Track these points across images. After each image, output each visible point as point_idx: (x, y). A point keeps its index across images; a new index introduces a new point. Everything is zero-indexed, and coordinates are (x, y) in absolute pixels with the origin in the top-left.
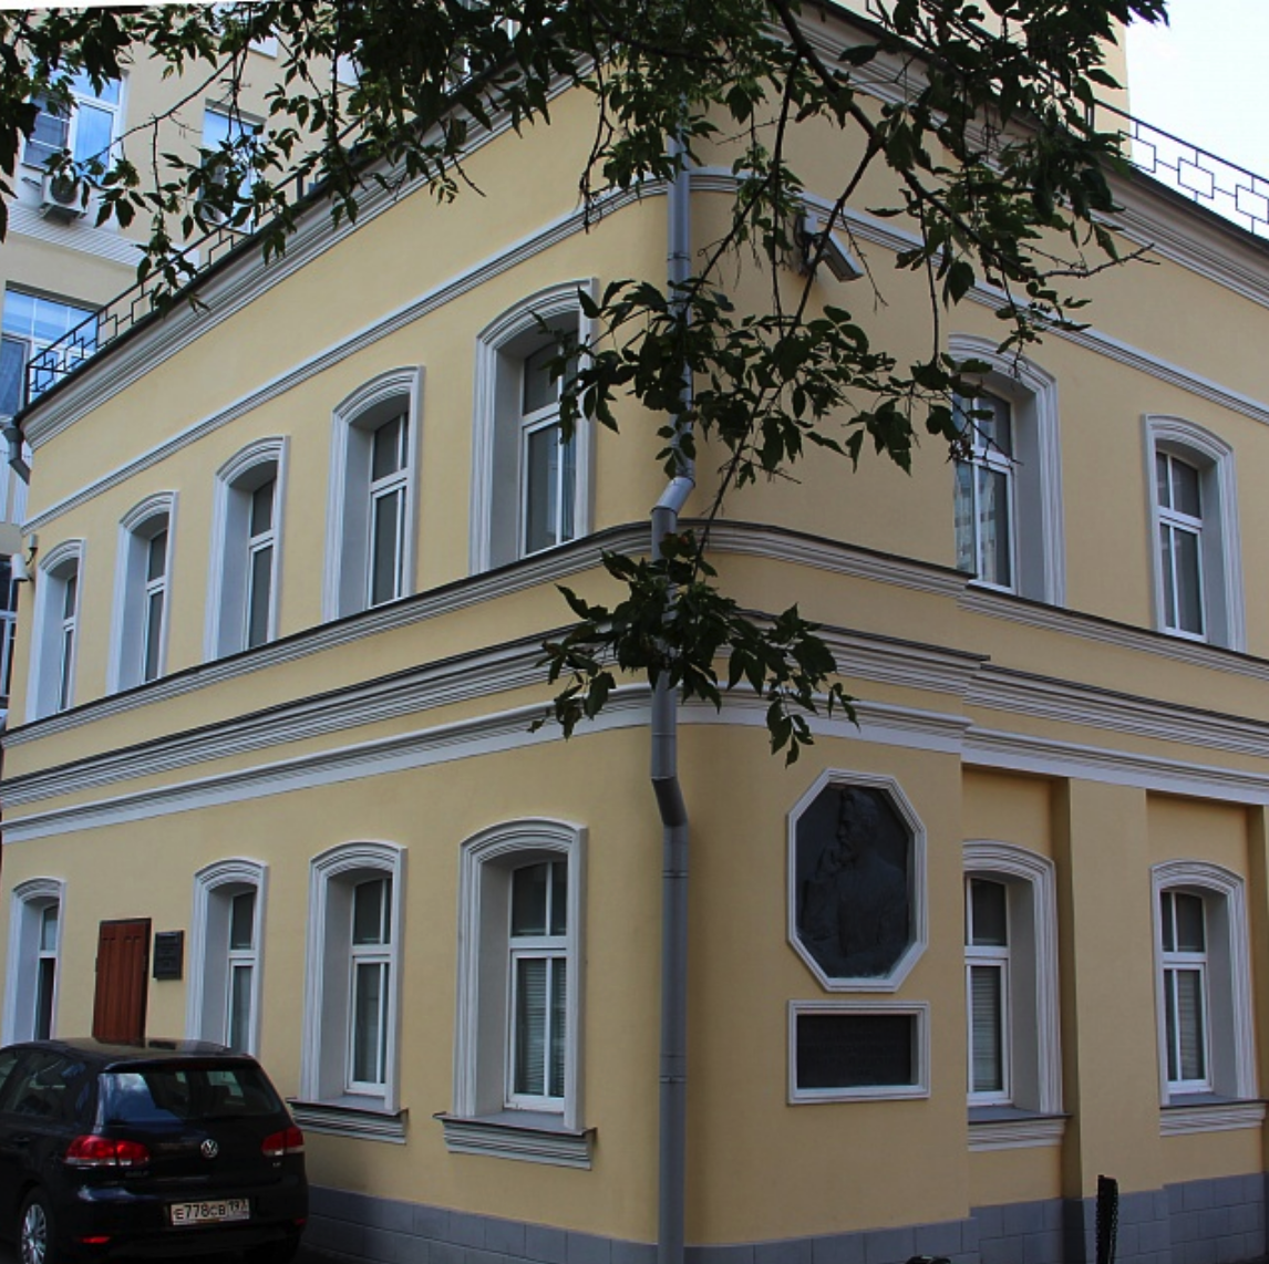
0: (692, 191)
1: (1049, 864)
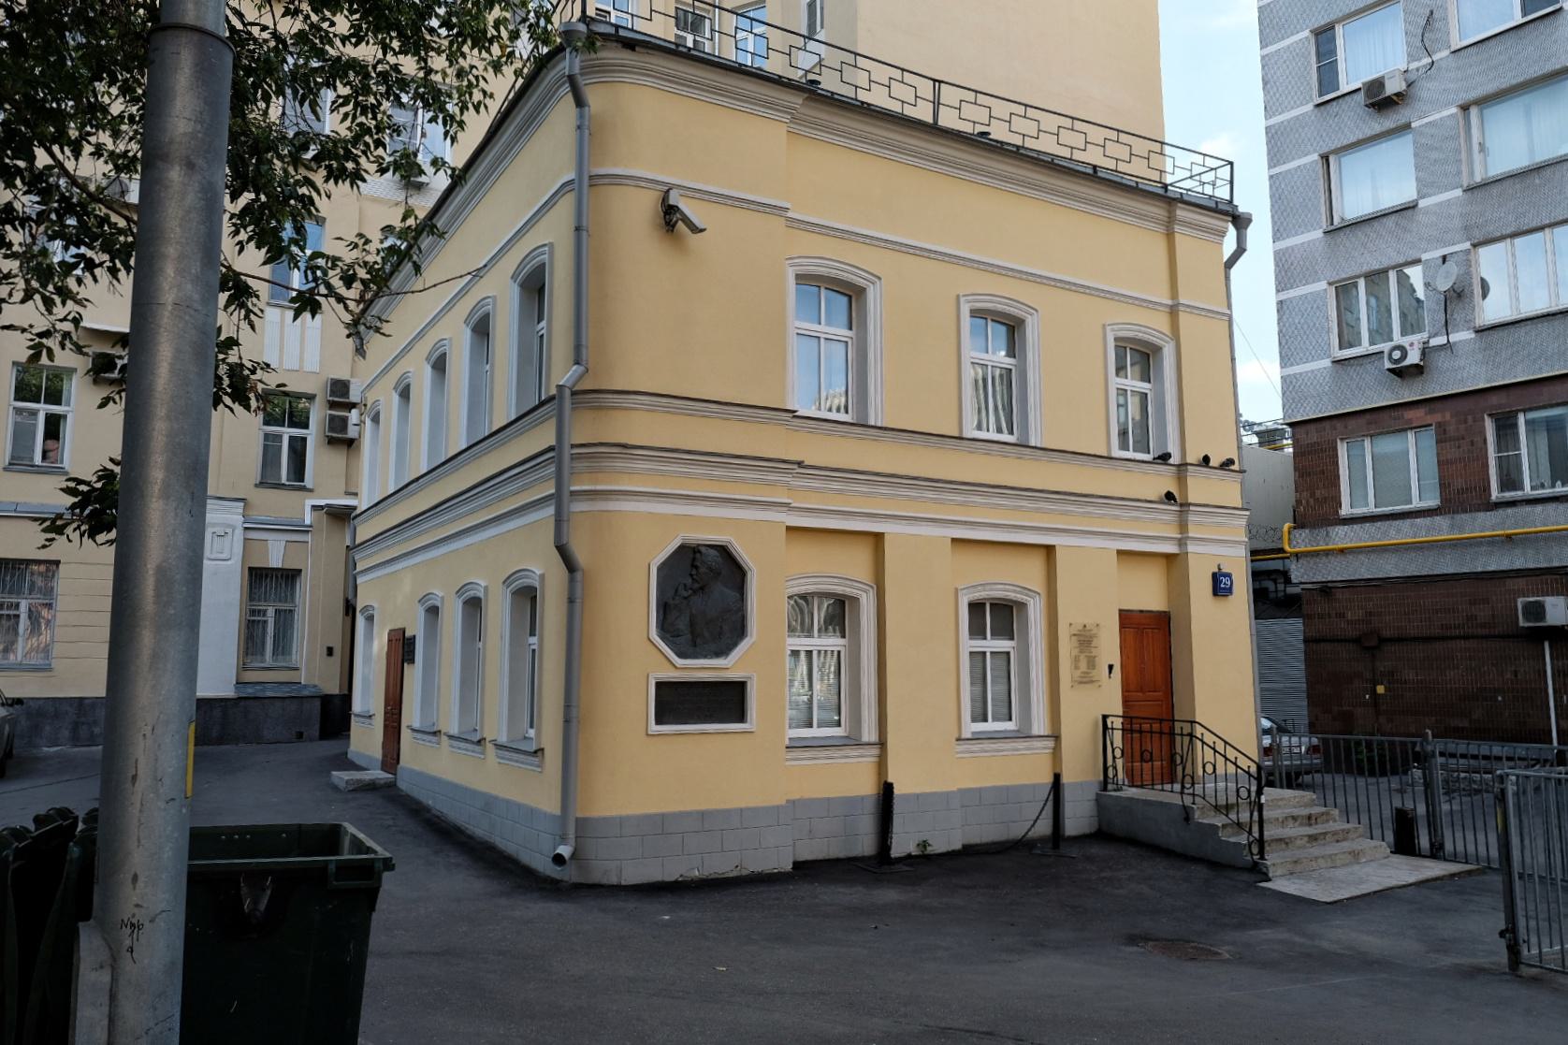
0: (591, 186)
1: (872, 587)
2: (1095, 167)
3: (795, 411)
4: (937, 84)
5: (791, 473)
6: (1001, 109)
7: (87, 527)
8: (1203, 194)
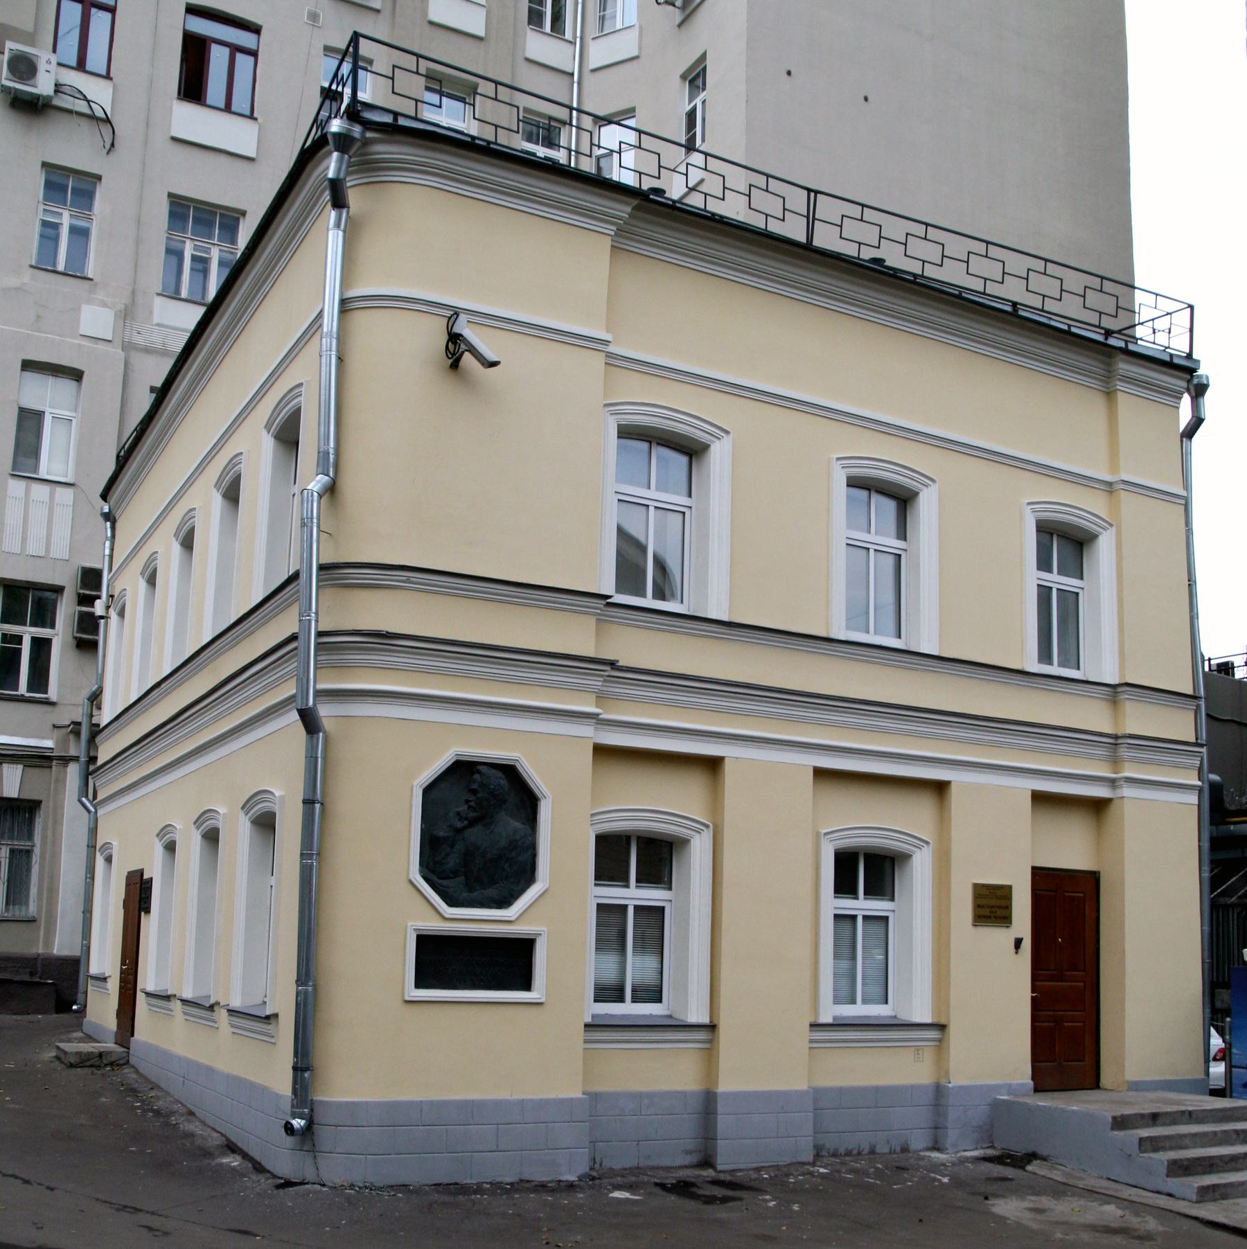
2: (1014, 304)
3: (610, 597)
4: (812, 195)
5: (602, 676)
6: (896, 229)
8: (1154, 343)
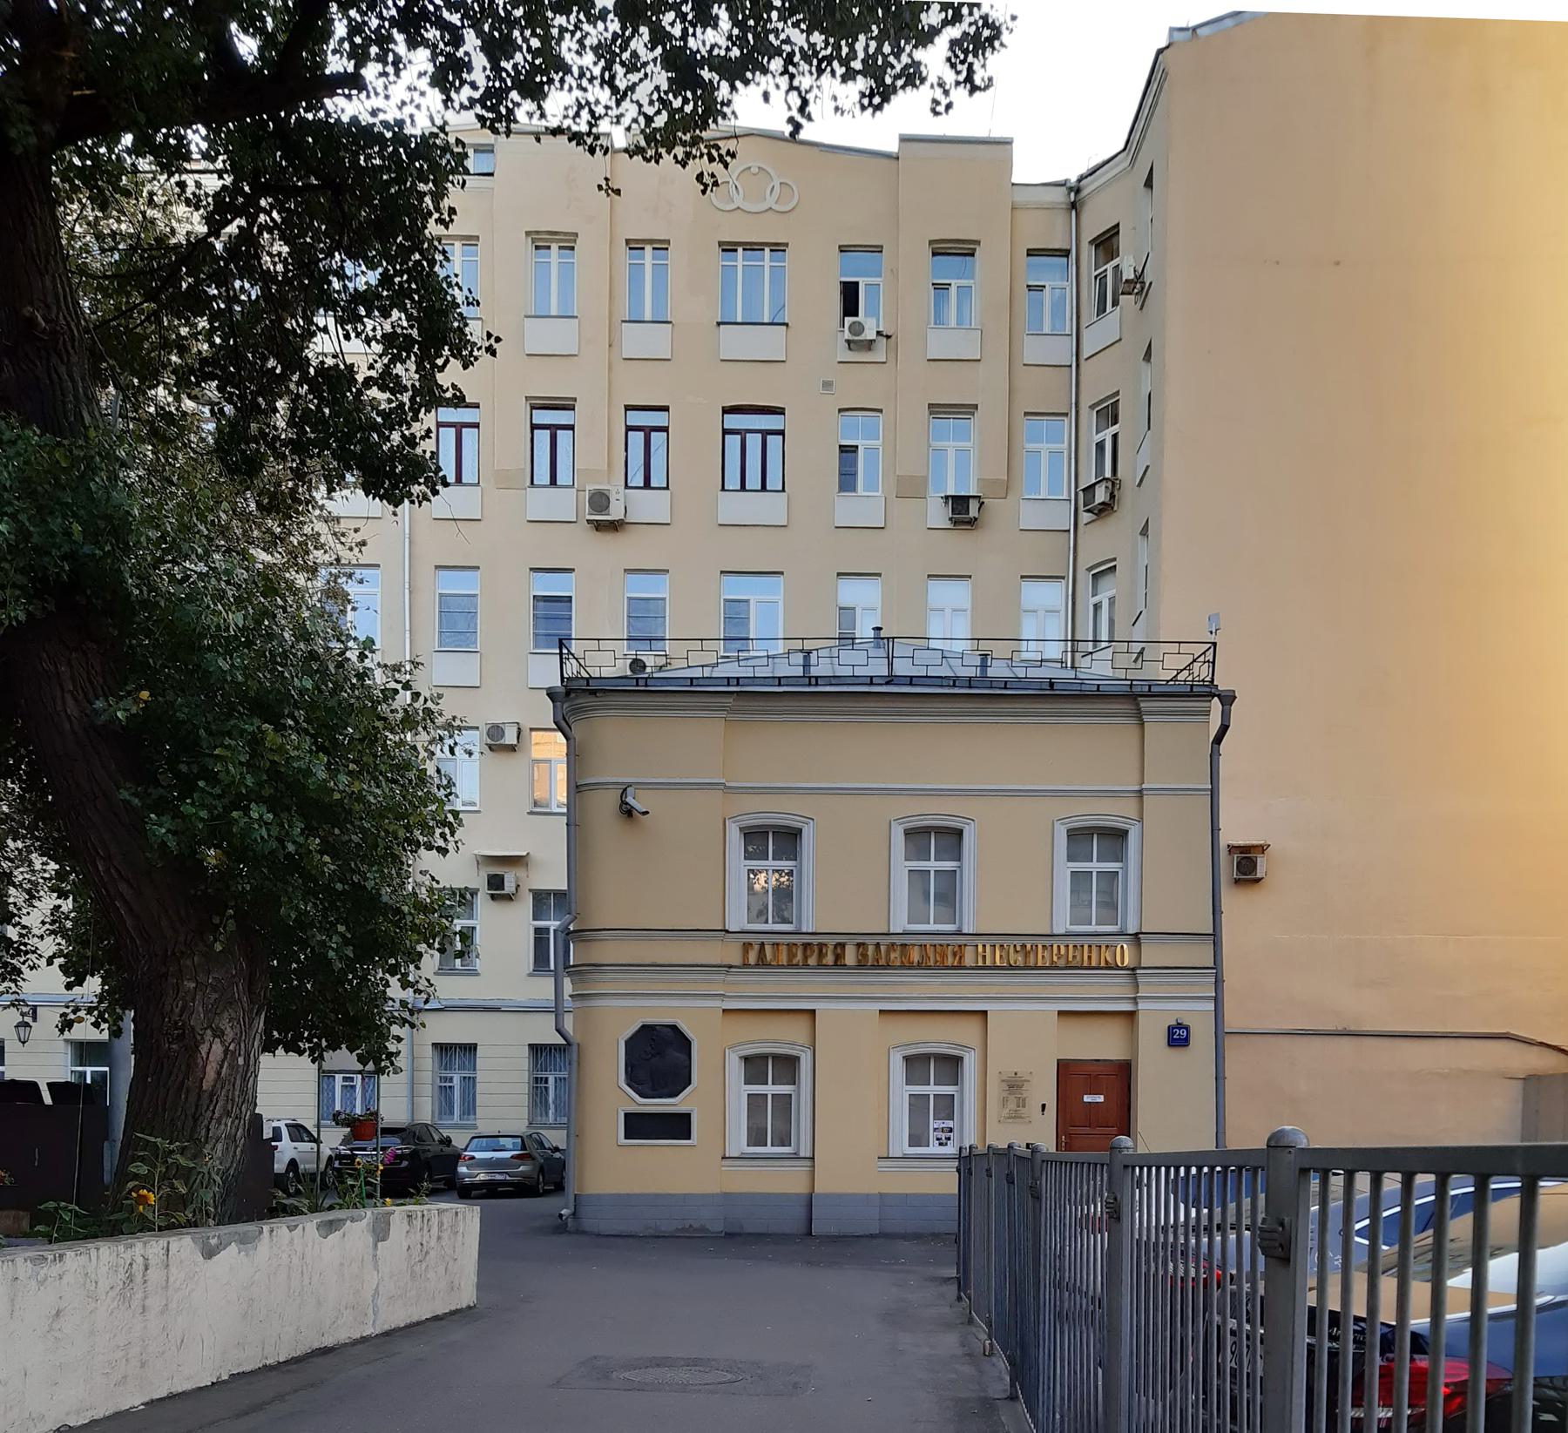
7: (17, 153)
